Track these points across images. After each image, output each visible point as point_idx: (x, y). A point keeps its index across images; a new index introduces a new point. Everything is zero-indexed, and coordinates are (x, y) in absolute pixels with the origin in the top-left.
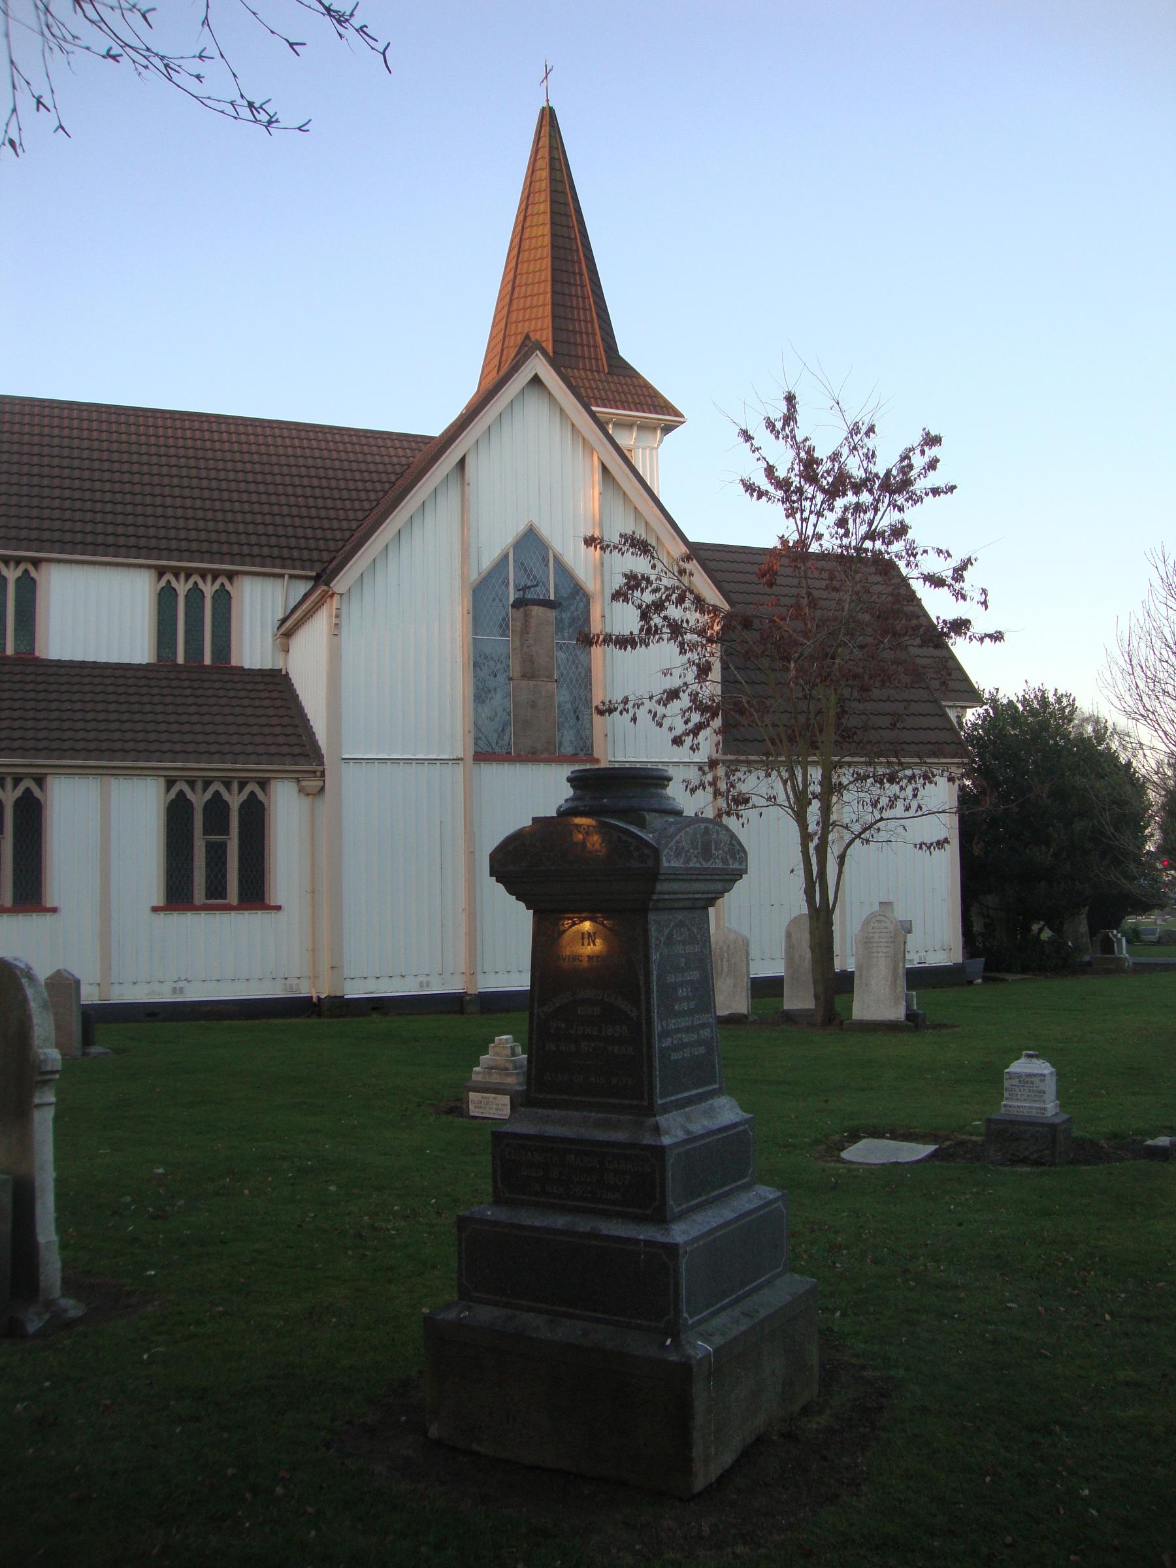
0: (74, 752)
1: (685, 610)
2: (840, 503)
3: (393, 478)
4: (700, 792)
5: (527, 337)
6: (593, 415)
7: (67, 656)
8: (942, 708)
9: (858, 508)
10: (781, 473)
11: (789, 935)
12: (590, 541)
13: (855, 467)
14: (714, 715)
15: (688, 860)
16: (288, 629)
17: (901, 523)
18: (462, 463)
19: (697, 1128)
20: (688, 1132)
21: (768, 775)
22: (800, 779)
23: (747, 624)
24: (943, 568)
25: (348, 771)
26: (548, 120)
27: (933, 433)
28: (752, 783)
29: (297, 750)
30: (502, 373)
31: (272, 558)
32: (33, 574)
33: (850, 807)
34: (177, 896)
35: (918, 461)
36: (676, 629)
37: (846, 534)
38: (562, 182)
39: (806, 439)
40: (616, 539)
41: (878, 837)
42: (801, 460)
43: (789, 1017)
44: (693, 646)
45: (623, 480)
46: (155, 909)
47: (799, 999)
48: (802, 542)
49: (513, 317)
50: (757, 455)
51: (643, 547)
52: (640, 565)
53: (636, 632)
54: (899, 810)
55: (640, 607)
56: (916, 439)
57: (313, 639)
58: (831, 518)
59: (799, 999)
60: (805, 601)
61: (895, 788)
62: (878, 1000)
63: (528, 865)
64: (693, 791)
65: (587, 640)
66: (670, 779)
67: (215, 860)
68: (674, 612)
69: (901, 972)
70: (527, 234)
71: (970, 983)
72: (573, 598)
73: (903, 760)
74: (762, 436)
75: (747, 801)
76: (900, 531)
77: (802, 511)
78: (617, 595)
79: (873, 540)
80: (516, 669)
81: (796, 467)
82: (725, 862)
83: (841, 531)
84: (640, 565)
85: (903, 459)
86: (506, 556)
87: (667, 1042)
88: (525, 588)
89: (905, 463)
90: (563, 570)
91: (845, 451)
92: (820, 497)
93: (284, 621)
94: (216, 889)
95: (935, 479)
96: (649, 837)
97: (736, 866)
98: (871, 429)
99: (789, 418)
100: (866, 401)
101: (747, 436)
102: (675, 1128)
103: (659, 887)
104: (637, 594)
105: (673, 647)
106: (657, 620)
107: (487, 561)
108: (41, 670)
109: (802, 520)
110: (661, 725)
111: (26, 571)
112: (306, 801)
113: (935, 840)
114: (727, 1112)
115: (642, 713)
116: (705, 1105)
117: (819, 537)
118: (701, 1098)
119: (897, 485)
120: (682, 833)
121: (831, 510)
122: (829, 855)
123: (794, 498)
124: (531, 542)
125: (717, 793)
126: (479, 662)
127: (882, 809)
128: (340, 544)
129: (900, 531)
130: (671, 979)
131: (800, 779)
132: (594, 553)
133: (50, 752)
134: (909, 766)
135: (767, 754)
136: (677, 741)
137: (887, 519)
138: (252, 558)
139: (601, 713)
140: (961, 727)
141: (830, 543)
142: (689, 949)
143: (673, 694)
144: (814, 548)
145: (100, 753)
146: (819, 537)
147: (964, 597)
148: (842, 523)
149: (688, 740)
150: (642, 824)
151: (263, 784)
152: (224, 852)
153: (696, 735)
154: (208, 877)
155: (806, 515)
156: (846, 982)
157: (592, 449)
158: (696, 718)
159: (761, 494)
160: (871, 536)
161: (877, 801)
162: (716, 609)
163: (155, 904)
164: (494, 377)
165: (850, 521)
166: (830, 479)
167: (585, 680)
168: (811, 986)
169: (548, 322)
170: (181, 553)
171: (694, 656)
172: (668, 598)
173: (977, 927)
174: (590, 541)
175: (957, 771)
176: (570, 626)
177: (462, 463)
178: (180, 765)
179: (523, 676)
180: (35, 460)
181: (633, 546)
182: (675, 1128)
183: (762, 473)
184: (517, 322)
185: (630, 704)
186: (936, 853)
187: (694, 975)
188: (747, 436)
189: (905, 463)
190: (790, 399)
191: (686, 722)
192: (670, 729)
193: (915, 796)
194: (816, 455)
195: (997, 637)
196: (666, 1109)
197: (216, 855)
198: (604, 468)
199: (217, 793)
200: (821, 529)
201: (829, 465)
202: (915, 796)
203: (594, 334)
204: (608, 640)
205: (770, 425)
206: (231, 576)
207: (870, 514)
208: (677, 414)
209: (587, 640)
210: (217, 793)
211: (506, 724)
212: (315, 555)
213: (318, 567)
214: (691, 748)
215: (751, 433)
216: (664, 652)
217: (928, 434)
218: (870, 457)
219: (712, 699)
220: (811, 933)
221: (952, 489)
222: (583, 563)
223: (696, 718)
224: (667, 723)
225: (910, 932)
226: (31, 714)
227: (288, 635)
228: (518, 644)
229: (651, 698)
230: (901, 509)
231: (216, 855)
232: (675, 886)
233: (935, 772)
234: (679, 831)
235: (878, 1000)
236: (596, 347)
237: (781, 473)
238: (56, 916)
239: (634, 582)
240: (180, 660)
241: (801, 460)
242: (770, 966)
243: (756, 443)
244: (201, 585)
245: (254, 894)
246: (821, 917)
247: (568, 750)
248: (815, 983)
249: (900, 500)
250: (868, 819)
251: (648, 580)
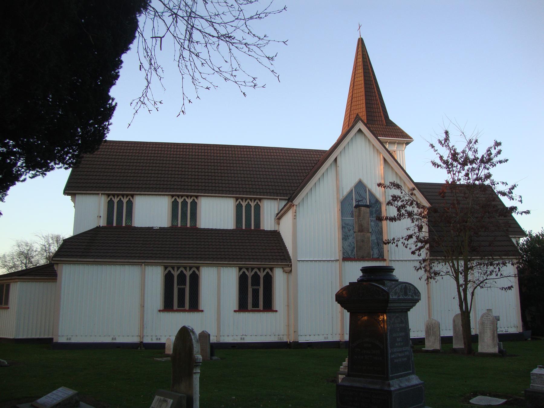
0: (209, 259)
1: (413, 207)
2: (466, 168)
3: (313, 165)
4: (420, 270)
5: (358, 115)
6: (379, 140)
7: (207, 227)
8: (510, 238)
9: (473, 169)
10: (445, 158)
11: (454, 321)
12: (379, 185)
13: (471, 156)
14: (426, 243)
15: (399, 296)
16: (279, 217)
17: (489, 173)
18: (336, 160)
19: (403, 385)
20: (400, 386)
21: (445, 264)
22: (456, 265)
23: (435, 211)
24: (505, 189)
25: (300, 265)
26: (361, 42)
27: (498, 142)
28: (438, 267)
29: (282, 257)
30: (350, 126)
31: (274, 193)
32: (196, 200)
33: (475, 275)
34: (243, 307)
35: (494, 152)
36: (410, 214)
37: (469, 179)
38: (367, 62)
39: (453, 146)
40: (388, 184)
41: (486, 285)
42: (452, 154)
43: (455, 351)
44: (417, 219)
45: (391, 162)
46: (235, 311)
47: (458, 345)
48: (454, 181)
49: (353, 108)
50: (436, 152)
51: (398, 186)
52: (397, 192)
53: (396, 216)
54: (494, 276)
55: (397, 207)
56: (492, 144)
57: (288, 219)
58: (464, 173)
59: (458, 345)
60: (455, 202)
61: (491, 268)
62: (487, 345)
63: (347, 297)
64: (418, 270)
65: (380, 219)
66: (394, 269)
67: (256, 295)
68: (409, 208)
69: (496, 335)
70: (356, 80)
71: (526, 340)
72: (375, 204)
73: (494, 257)
74: (438, 146)
75: (439, 274)
76: (488, 176)
77: (453, 171)
78: (389, 203)
79: (478, 180)
80: (356, 229)
81: (450, 156)
82: (412, 296)
83: (467, 178)
84: (397, 192)
85: (488, 151)
86: (352, 190)
87: (393, 356)
88: (359, 201)
89: (489, 152)
90: (371, 194)
91: (467, 150)
92: (459, 166)
93: (278, 214)
94: (256, 305)
95: (500, 157)
96: (386, 289)
97: (417, 298)
98: (476, 141)
99: (447, 139)
100: (474, 130)
101: (432, 146)
102: (395, 385)
103: (389, 305)
104: (396, 202)
105: (409, 220)
106: (403, 211)
107: (345, 193)
108: (198, 232)
109: (453, 174)
110: (406, 247)
111: (194, 199)
112: (285, 275)
113: (507, 286)
114: (415, 380)
115: (400, 243)
116: (407, 378)
117: (459, 180)
118: (405, 375)
119: (487, 160)
120: (397, 288)
121: (463, 170)
122: (468, 293)
123: (450, 167)
124: (360, 185)
125: (425, 271)
126: (344, 227)
127: (487, 276)
128: (296, 188)
129: (488, 176)
130: (394, 335)
131: (456, 265)
132: (382, 189)
133: (201, 259)
134: (497, 260)
135: (445, 257)
136: (413, 253)
137: (483, 173)
138: (267, 194)
139: (385, 244)
140: (518, 245)
141: (463, 182)
142: (401, 325)
143: (410, 237)
144: (458, 183)
145: (217, 259)
146: (459, 180)
147: (513, 199)
148: (467, 175)
149: (417, 252)
150: (384, 284)
151: (271, 269)
152: (258, 292)
153: (420, 250)
154: (253, 300)
155: (454, 172)
156: (475, 339)
157: (380, 153)
158: (419, 245)
159: (438, 166)
160: (477, 179)
161: (486, 272)
162: (423, 207)
163: (235, 309)
164: (347, 129)
165: (470, 174)
166: (462, 160)
167: (381, 233)
168: (462, 339)
169: (364, 109)
170: (243, 192)
171: (417, 223)
172: (407, 204)
173: (528, 319)
174: (379, 185)
175: (515, 261)
176: (375, 213)
177: (336, 160)
178: (243, 263)
179: (359, 231)
180: (197, 163)
181: (394, 186)
182: (395, 385)
183: (439, 159)
184: (354, 110)
185: (395, 241)
186: (509, 291)
187: (403, 334)
188: (432, 146)
189: (489, 152)
190: (447, 133)
191: (416, 246)
192: (410, 249)
193: (499, 270)
194: (457, 151)
195: (528, 212)
196: (392, 378)
197: (256, 293)
198: (385, 159)
199: (256, 272)
200: (460, 177)
201: (462, 154)
202: (499, 270)
203: (380, 112)
204: (387, 218)
205: (440, 142)
206: (260, 200)
207: (477, 171)
208: (410, 138)
209: (380, 219)
210: (256, 272)
211: (354, 248)
212: (288, 192)
213: (289, 196)
214: (418, 255)
215: (434, 145)
216: (406, 222)
217: (496, 142)
218: (476, 151)
219: (424, 238)
220: (462, 321)
221: (507, 160)
222: (378, 192)
223: (419, 245)
224: (409, 246)
225: (499, 320)
226: (195, 246)
227: (279, 219)
228: (357, 220)
229: (402, 238)
230: (488, 169)
231: (256, 293)
232: (395, 305)
233: (507, 262)
234: (396, 286)
235: (487, 345)
236: (381, 117)
237: (445, 158)
238: (202, 313)
239: (395, 198)
240: (244, 228)
241: (452, 154)
242: (447, 331)
243: (436, 148)
244: (250, 203)
245: (268, 307)
246: (465, 315)
247: (376, 256)
248: (464, 338)
249: (488, 166)
250: (481, 279)
251: (400, 198)
